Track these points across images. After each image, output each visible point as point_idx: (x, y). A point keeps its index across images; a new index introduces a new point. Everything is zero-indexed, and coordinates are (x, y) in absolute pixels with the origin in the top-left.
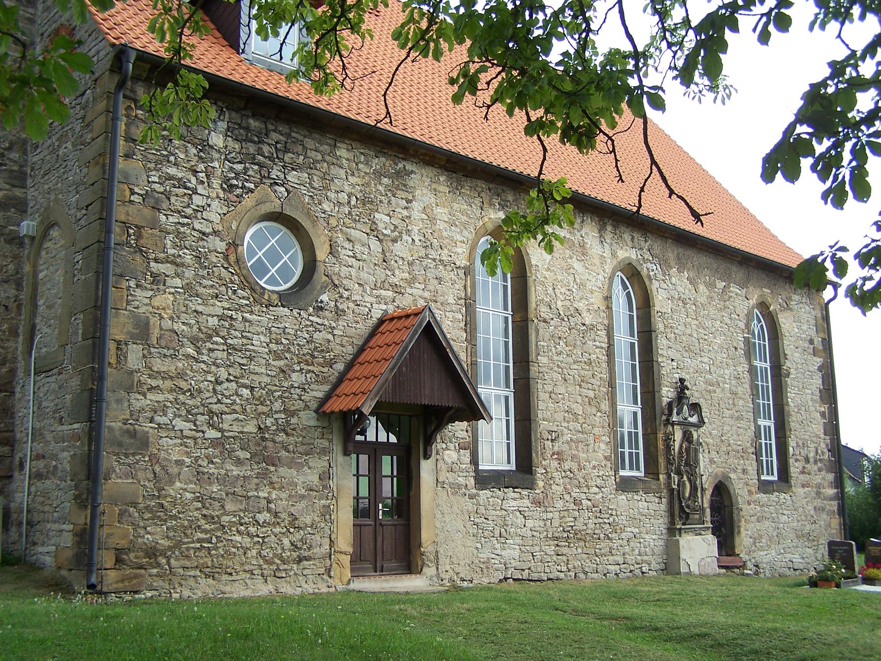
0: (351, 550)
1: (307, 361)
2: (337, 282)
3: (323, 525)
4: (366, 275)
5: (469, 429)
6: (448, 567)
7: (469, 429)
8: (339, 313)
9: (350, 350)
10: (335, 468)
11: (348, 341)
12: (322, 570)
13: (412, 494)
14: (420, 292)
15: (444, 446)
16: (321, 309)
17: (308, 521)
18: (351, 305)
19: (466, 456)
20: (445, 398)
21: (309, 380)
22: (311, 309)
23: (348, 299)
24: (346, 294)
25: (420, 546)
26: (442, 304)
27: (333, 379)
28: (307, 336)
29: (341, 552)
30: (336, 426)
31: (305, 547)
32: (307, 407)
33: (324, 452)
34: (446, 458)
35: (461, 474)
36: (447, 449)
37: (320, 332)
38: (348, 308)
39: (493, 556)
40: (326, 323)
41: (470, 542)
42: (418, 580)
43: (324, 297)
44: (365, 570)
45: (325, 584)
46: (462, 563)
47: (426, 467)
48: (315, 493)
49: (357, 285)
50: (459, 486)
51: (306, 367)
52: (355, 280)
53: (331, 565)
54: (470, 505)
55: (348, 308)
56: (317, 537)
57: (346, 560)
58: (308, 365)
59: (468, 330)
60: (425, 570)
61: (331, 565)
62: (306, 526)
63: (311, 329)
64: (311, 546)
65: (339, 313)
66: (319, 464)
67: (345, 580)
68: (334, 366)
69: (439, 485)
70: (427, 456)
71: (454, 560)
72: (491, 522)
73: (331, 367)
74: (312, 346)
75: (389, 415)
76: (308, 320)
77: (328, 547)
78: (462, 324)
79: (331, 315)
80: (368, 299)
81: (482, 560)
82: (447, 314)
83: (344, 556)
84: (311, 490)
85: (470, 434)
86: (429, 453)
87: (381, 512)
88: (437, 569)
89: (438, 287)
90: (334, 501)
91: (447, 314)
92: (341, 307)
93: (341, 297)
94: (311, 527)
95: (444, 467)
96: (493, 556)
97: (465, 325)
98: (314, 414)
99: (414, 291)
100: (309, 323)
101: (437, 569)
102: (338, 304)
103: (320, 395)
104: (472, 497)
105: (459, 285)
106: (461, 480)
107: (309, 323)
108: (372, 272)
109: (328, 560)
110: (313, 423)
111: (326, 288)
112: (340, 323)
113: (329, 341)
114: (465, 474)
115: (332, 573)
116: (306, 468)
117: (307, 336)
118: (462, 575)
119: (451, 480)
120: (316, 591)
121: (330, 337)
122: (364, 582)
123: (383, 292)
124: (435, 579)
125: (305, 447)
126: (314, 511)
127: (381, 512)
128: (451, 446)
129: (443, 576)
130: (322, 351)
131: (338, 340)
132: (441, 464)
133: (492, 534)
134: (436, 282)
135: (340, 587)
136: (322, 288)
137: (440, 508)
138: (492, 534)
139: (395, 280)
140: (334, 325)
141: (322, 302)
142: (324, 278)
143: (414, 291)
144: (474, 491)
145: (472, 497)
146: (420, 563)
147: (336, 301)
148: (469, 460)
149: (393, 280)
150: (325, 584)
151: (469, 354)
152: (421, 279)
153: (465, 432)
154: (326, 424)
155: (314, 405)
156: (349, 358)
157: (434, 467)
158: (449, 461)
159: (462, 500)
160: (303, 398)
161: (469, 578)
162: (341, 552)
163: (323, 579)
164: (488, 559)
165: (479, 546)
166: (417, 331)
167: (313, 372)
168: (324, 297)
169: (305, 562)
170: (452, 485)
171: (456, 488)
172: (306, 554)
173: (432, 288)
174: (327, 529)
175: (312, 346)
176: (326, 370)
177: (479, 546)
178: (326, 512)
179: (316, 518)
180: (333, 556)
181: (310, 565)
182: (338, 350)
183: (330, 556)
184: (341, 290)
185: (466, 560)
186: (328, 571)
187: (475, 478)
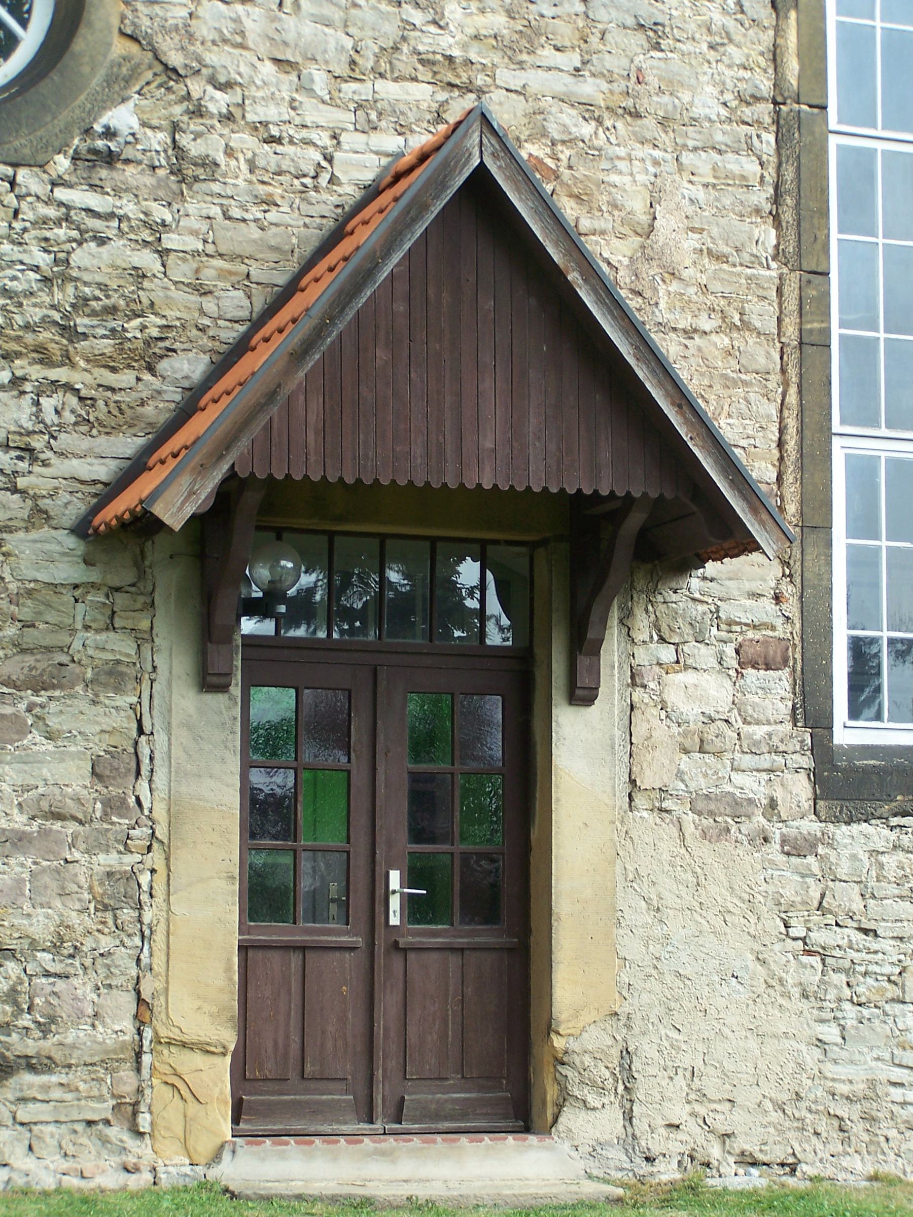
0: (229, 1038)
1: (40, 349)
2: (175, 59)
3: (106, 943)
4: (309, 29)
5: (788, 589)
6: (678, 1112)
7: (788, 589)
8: (186, 171)
9: (236, 303)
10: (160, 738)
11: (222, 274)
12: (103, 1109)
13: (534, 835)
14: (562, 83)
15: (667, 654)
16: (110, 159)
17: (40, 925)
18: (245, 141)
19: (774, 692)
20: (602, 470)
21: (50, 417)
22: (62, 163)
23: (228, 118)
24: (218, 101)
25: (549, 1029)
26: (664, 123)
27: (156, 413)
28: (43, 259)
29: (184, 1045)
30: (168, 580)
31: (25, 1020)
32: (40, 516)
33: (113, 676)
34: (674, 697)
35: (747, 761)
36: (680, 664)
37: (102, 241)
38: (229, 152)
39: (898, 1074)
40: (129, 207)
41: (793, 1020)
42: (533, 1155)
43: (122, 117)
44: (317, 1111)
45: (115, 1160)
46: (747, 1097)
47: (579, 743)
48: (72, 827)
49: (268, 68)
50: (739, 808)
51: (36, 372)
52: (264, 49)
53: (140, 1091)
54: (790, 881)
55: (229, 152)
56: (82, 987)
57: (215, 1077)
58: (46, 361)
59: (788, 216)
60: (570, 1118)
61: (140, 1091)
62: (34, 945)
63: (62, 232)
64: (53, 1019)
65: (186, 171)
66: (92, 721)
67: (204, 1146)
68: (163, 366)
69: (639, 800)
70: (582, 695)
71: (712, 1085)
72: (885, 945)
73: (151, 369)
74: (65, 296)
75: (331, 535)
76: (49, 201)
77: (128, 1025)
78: (762, 197)
79: (149, 180)
80: (314, 112)
81: (844, 1089)
82: (687, 158)
83: (198, 1059)
84: (58, 816)
85: (792, 607)
86: (583, 680)
87: (395, 903)
88: (629, 1117)
89: (651, 62)
90: (156, 858)
91: (687, 158)
92: (195, 149)
93: (198, 112)
94: (55, 948)
95: (663, 732)
96: (898, 1074)
97: (777, 199)
98: (71, 542)
99: (534, 80)
100: (51, 212)
101: (629, 1117)
102: (184, 140)
103: (103, 471)
104: (795, 848)
105: (751, 46)
106: (751, 785)
107: (51, 212)
108: (337, 15)
109: (126, 1074)
110: (68, 571)
111: (128, 81)
112: (192, 207)
113: (139, 275)
114: (765, 761)
115: (144, 1121)
116: (36, 736)
117: (43, 259)
118: (742, 1143)
119: (700, 784)
120: (73, 1182)
121: (148, 260)
122: (283, 1156)
123: (388, 89)
124: (617, 1155)
125: (29, 660)
126: (63, 894)
127: (395, 903)
128: (704, 655)
129: (655, 1143)
130: (112, 310)
131: (181, 271)
132: (649, 722)
133: (893, 991)
134: (639, 39)
135: (175, 1168)
136: (110, 81)
137: (644, 888)
138: (893, 991)
139: (448, 43)
140: (161, 213)
141: (109, 133)
142: (120, 47)
143: (534, 80)
144: (810, 826)
145: (795, 848)
146: (552, 1093)
147: (175, 128)
148: (784, 709)
149: (432, 41)
150: (115, 1160)
151: (791, 305)
152: (565, 33)
153: (768, 604)
154: (125, 576)
155: (72, 508)
156: (231, 334)
157: (619, 734)
158: (691, 711)
159: (749, 859)
160: (21, 482)
161: (778, 1153)
162: (184, 1045)
163: (105, 1141)
164: (872, 1084)
165: (831, 1033)
166: (424, 208)
167: (69, 388)
168: (122, 117)
169: (27, 1078)
170: (701, 804)
171: (722, 813)
172: (31, 1046)
173: (614, 63)
174: (124, 960)
175: (65, 296)
176: (126, 378)
177: (831, 1033)
178: (119, 897)
179: (74, 919)
180: (146, 1059)
181: (46, 1088)
182: (179, 305)
183: (138, 1055)
184: (196, 87)
185: (769, 1089)
186: (129, 1112)
187: (816, 777)
